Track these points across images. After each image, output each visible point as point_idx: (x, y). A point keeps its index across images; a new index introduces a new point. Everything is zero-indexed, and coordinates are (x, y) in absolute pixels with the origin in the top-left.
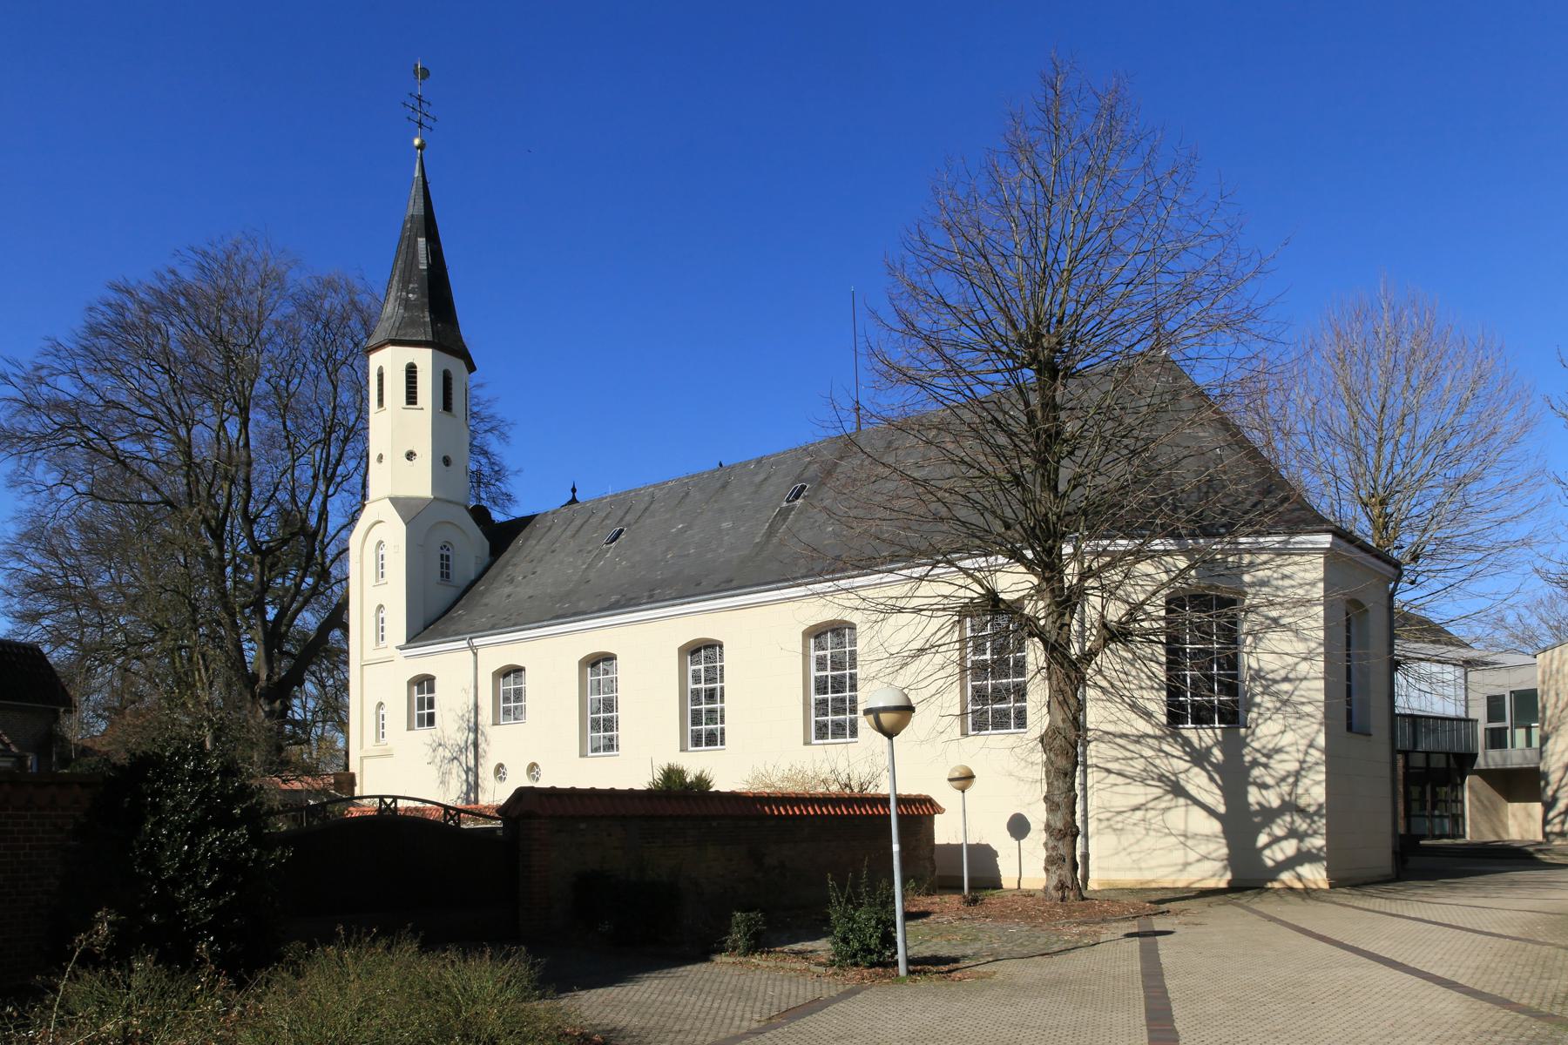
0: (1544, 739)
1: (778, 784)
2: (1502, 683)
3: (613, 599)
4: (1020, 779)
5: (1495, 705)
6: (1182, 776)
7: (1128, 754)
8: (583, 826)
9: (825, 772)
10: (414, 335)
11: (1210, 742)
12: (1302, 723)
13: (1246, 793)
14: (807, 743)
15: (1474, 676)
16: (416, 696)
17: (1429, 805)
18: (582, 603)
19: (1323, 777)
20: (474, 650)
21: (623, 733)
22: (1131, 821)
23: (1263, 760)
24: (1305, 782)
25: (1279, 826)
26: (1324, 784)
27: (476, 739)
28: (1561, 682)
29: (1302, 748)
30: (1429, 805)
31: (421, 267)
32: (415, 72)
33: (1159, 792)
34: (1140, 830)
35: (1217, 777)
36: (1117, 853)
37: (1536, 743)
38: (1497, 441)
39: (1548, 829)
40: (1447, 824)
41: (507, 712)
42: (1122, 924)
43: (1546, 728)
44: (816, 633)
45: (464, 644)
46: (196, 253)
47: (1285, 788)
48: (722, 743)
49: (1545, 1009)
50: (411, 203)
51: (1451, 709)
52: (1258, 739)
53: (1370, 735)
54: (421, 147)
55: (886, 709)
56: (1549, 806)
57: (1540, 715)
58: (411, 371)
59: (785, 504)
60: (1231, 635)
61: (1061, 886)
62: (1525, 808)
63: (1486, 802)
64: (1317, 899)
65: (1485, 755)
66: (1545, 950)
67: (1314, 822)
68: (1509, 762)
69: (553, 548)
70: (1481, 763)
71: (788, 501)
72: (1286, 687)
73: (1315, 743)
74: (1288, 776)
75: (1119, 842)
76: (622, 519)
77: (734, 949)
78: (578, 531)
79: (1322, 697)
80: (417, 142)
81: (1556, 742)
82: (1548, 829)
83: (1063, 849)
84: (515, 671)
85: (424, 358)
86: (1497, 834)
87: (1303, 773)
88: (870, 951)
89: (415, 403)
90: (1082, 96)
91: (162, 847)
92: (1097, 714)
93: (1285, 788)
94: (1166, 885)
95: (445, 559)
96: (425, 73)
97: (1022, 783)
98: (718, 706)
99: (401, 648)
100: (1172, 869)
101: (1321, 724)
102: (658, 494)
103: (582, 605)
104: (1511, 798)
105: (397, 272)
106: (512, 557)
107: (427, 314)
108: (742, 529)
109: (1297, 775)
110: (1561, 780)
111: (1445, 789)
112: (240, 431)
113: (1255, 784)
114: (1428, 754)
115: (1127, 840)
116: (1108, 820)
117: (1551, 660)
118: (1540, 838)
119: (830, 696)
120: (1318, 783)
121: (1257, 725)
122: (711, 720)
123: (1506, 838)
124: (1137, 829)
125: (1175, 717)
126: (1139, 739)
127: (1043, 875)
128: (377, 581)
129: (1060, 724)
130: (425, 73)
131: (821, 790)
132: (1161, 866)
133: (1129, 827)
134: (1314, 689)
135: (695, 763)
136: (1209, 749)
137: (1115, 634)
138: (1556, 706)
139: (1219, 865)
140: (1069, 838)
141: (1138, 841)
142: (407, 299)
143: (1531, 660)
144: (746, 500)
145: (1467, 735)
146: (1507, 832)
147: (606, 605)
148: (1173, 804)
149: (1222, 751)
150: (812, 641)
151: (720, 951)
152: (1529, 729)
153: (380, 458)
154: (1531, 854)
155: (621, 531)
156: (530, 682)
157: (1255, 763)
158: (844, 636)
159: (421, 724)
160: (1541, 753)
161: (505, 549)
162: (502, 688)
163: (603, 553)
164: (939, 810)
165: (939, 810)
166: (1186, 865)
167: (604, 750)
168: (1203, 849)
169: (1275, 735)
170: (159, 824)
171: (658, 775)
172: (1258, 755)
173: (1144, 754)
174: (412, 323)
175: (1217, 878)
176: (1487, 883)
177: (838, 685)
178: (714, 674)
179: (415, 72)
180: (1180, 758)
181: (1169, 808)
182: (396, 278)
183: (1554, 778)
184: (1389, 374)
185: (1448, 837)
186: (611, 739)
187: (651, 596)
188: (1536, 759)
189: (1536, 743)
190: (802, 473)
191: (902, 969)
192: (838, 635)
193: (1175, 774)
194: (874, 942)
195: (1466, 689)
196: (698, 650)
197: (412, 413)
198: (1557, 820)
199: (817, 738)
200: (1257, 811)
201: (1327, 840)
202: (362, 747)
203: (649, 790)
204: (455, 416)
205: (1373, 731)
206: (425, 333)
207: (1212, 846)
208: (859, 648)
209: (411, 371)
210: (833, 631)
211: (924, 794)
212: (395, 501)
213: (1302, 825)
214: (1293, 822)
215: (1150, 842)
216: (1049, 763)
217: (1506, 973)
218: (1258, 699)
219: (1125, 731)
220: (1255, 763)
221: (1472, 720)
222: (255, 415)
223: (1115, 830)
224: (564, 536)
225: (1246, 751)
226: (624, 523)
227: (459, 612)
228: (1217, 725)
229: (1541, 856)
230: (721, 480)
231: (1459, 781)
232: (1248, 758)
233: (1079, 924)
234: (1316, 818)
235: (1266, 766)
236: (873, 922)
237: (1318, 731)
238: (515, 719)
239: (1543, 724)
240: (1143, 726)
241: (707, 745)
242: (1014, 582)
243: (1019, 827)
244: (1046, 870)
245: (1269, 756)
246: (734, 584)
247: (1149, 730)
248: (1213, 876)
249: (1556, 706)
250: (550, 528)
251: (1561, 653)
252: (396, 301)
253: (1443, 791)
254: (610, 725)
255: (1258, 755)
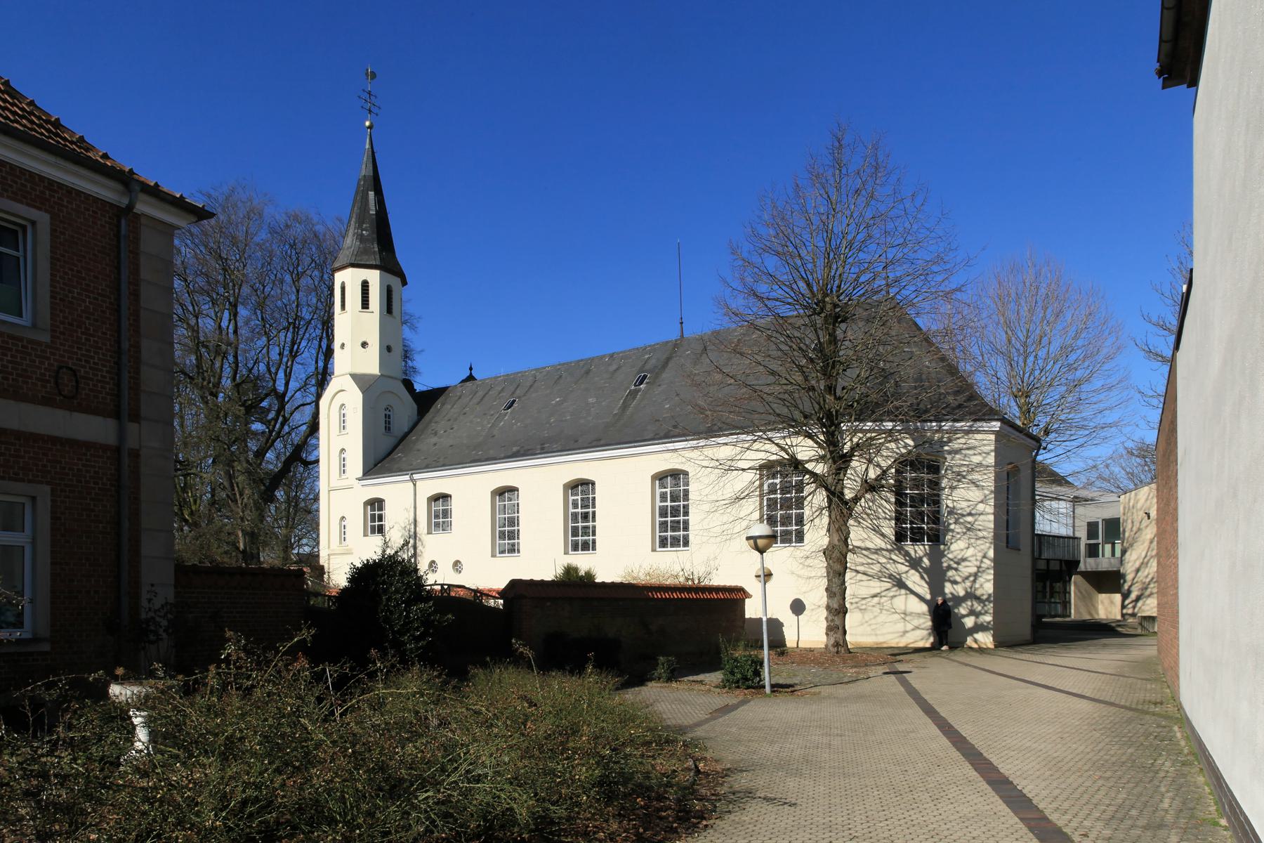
0: (1124, 552)
1: (642, 577)
2: (1098, 514)
3: (515, 449)
4: (799, 576)
5: (1092, 529)
6: (904, 575)
7: (870, 561)
8: (548, 604)
9: (676, 569)
10: (367, 260)
11: (921, 553)
12: (979, 542)
13: (943, 587)
14: (654, 550)
15: (1080, 510)
16: (369, 513)
17: (1048, 595)
18: (491, 452)
19: (992, 577)
20: (414, 482)
21: (524, 541)
22: (871, 604)
23: (955, 566)
24: (980, 580)
25: (964, 608)
26: (992, 582)
27: (415, 543)
28: (1135, 514)
29: (979, 558)
30: (1048, 595)
31: (371, 212)
32: (367, 74)
33: (889, 585)
34: (877, 610)
35: (925, 576)
36: (862, 624)
37: (1118, 554)
38: (1100, 357)
39: (1125, 611)
40: (1059, 608)
41: (437, 525)
42: (880, 667)
43: (1125, 544)
44: (661, 477)
45: (407, 477)
46: (203, 195)
47: (968, 584)
48: (594, 549)
49: (1134, 706)
50: (364, 167)
51: (1064, 531)
52: (952, 552)
53: (1019, 550)
54: (370, 127)
55: (760, 537)
56: (1125, 596)
57: (1121, 536)
58: (365, 286)
59: (633, 387)
60: (935, 485)
61: (837, 644)
62: (1109, 598)
63: (1084, 593)
64: (989, 654)
65: (1085, 562)
66: (1130, 680)
67: (985, 605)
68: (1100, 567)
69: (464, 411)
70: (1082, 567)
71: (635, 385)
72: (969, 519)
73: (987, 555)
74: (970, 576)
75: (863, 617)
76: (513, 393)
77: (659, 679)
78: (482, 400)
79: (992, 526)
80: (367, 124)
81: (1131, 555)
82: (1125, 611)
83: (838, 622)
84: (444, 497)
85: (373, 277)
86: (1090, 614)
87: (979, 574)
88: (747, 679)
89: (368, 308)
90: (856, 146)
91: (391, 613)
92: (858, 536)
93: (968, 584)
94: (893, 645)
95: (387, 416)
96: (373, 75)
97: (800, 579)
98: (591, 524)
99: (359, 479)
100: (896, 635)
101: (991, 543)
102: (539, 376)
103: (492, 453)
104: (1101, 591)
105: (354, 216)
106: (433, 417)
107: (376, 246)
108: (603, 403)
109: (976, 575)
110: (1133, 579)
111: (1058, 584)
112: (230, 320)
113: (949, 581)
114: (1048, 561)
115: (868, 616)
116: (857, 603)
117: (1129, 500)
118: (1119, 617)
119: (669, 519)
120: (989, 581)
121: (951, 543)
122: (585, 533)
123: (1097, 617)
124: (874, 609)
125: (900, 537)
126: (878, 551)
127: (825, 637)
128: (340, 432)
129: (837, 543)
130: (373, 75)
131: (676, 582)
132: (889, 633)
133: (870, 608)
134: (987, 521)
135: (583, 562)
136: (921, 559)
137: (871, 487)
138: (1131, 530)
139: (925, 633)
140: (841, 615)
141: (875, 617)
142: (362, 235)
143: (1118, 499)
144: (605, 383)
145: (1073, 547)
146: (1098, 614)
147: (510, 454)
148: (898, 593)
149: (929, 560)
150: (657, 482)
151: (651, 680)
152: (1113, 544)
153: (343, 346)
154: (1113, 627)
155: (514, 401)
156: (455, 505)
157: (949, 568)
158: (679, 479)
159: (373, 532)
160: (1121, 561)
161: (427, 411)
162: (433, 509)
163: (501, 418)
164: (749, 596)
165: (749, 596)
166: (905, 632)
167: (508, 553)
168: (916, 622)
169: (962, 550)
170: (389, 599)
171: (560, 571)
172: (952, 563)
173: (880, 561)
174: (365, 251)
175: (924, 641)
176: (1089, 646)
177: (675, 511)
178: (589, 502)
179: (367, 74)
180: (902, 564)
181: (895, 596)
182: (353, 220)
183: (1129, 577)
184: (1032, 311)
185: (1059, 616)
186: (513, 545)
187: (542, 449)
188: (1118, 565)
189: (1118, 554)
190: (643, 366)
191: (768, 689)
192: (675, 478)
193: (899, 574)
194: (750, 674)
195: (1074, 517)
196: (577, 486)
197: (365, 315)
198: (1130, 606)
199: (660, 547)
200: (950, 598)
201: (994, 618)
202: (329, 547)
203: (553, 581)
204: (395, 318)
205: (1021, 547)
206: (375, 259)
207: (922, 621)
208: (691, 488)
209: (365, 286)
210: (671, 476)
211: (739, 585)
212: (355, 377)
213: (978, 608)
214: (972, 605)
215: (883, 617)
216: (829, 568)
217: (1111, 691)
218: (952, 527)
219: (868, 546)
220: (949, 568)
221: (1077, 538)
222: (243, 312)
223: (861, 610)
224: (471, 403)
225: (944, 560)
226: (515, 395)
227: (398, 455)
228: (926, 543)
229: (1120, 629)
230: (585, 369)
231: (1067, 578)
232: (945, 565)
233: (852, 667)
234: (987, 603)
235: (956, 569)
236: (750, 662)
237: (990, 547)
238: (443, 530)
239: (1123, 542)
240: (879, 542)
241: (582, 550)
242: (805, 449)
243: (798, 607)
244: (827, 634)
245: (958, 563)
246: (602, 442)
247: (883, 545)
248: (922, 639)
249: (1131, 530)
250: (460, 397)
251: (1136, 495)
252: (354, 235)
253: (1058, 586)
254: (513, 535)
255: (952, 563)
